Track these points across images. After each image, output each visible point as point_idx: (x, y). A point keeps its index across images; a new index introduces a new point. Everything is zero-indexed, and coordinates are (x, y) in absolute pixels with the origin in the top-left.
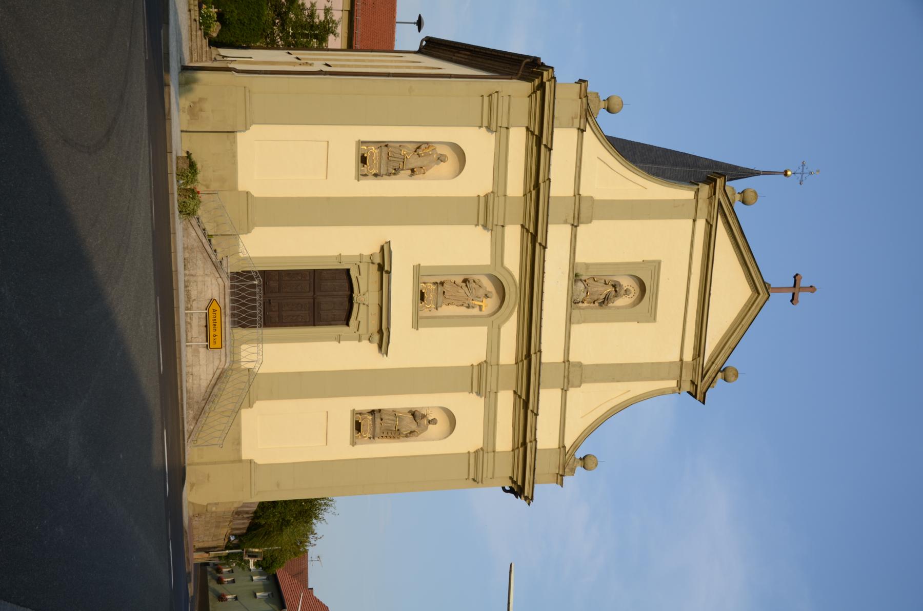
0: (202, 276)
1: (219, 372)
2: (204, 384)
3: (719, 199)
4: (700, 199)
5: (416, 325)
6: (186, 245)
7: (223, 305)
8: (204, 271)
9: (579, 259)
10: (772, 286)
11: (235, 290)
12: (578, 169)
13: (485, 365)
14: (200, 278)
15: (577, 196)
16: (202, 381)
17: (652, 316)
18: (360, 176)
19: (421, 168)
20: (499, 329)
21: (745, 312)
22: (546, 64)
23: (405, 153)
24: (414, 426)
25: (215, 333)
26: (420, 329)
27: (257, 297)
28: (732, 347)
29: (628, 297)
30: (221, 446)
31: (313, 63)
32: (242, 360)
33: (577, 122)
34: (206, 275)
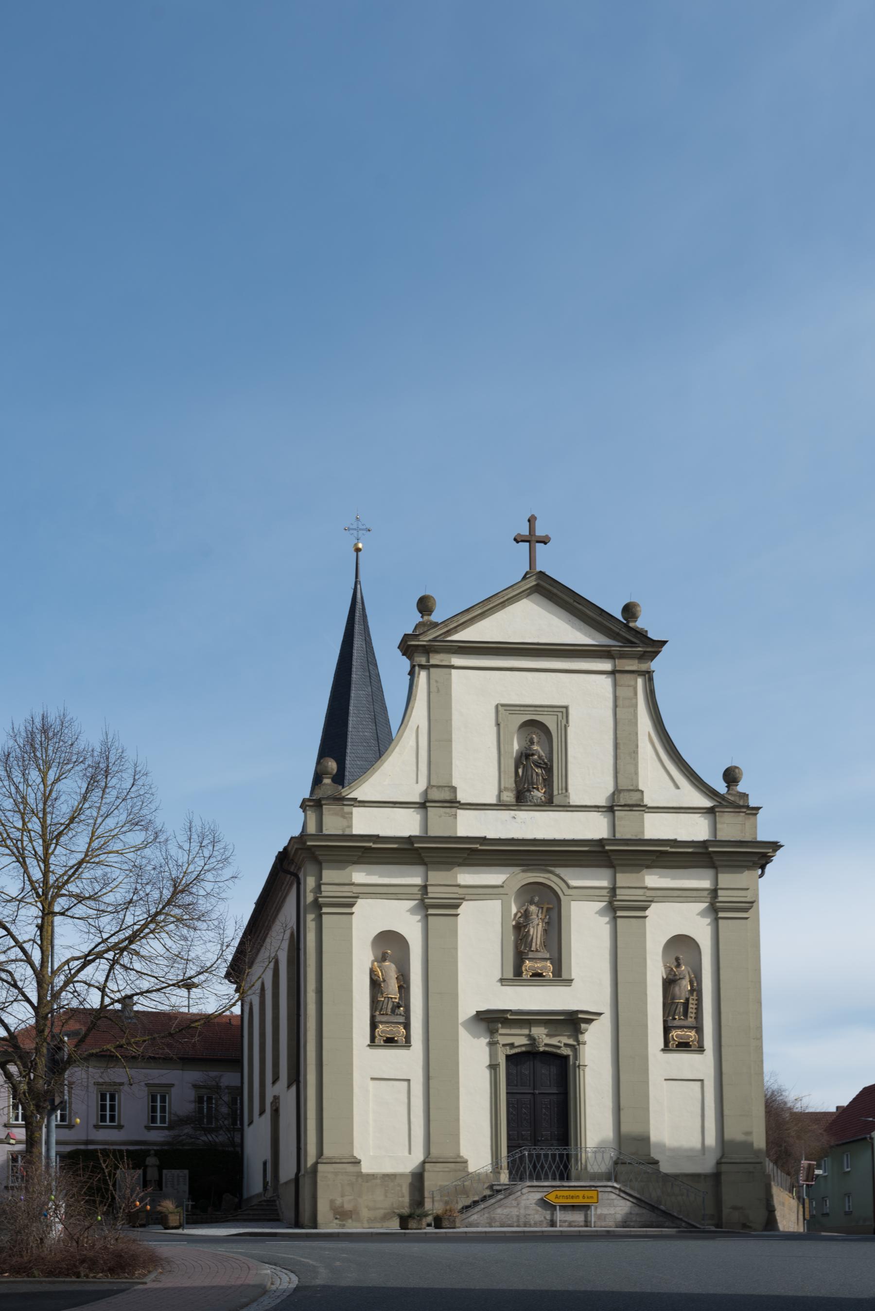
3: (430, 641)
5: (569, 982)
6: (487, 1225)
7: (550, 1188)
10: (528, 569)
12: (397, 805)
16: (633, 1212)
21: (518, 586)
22: (286, 845)
33: (346, 809)
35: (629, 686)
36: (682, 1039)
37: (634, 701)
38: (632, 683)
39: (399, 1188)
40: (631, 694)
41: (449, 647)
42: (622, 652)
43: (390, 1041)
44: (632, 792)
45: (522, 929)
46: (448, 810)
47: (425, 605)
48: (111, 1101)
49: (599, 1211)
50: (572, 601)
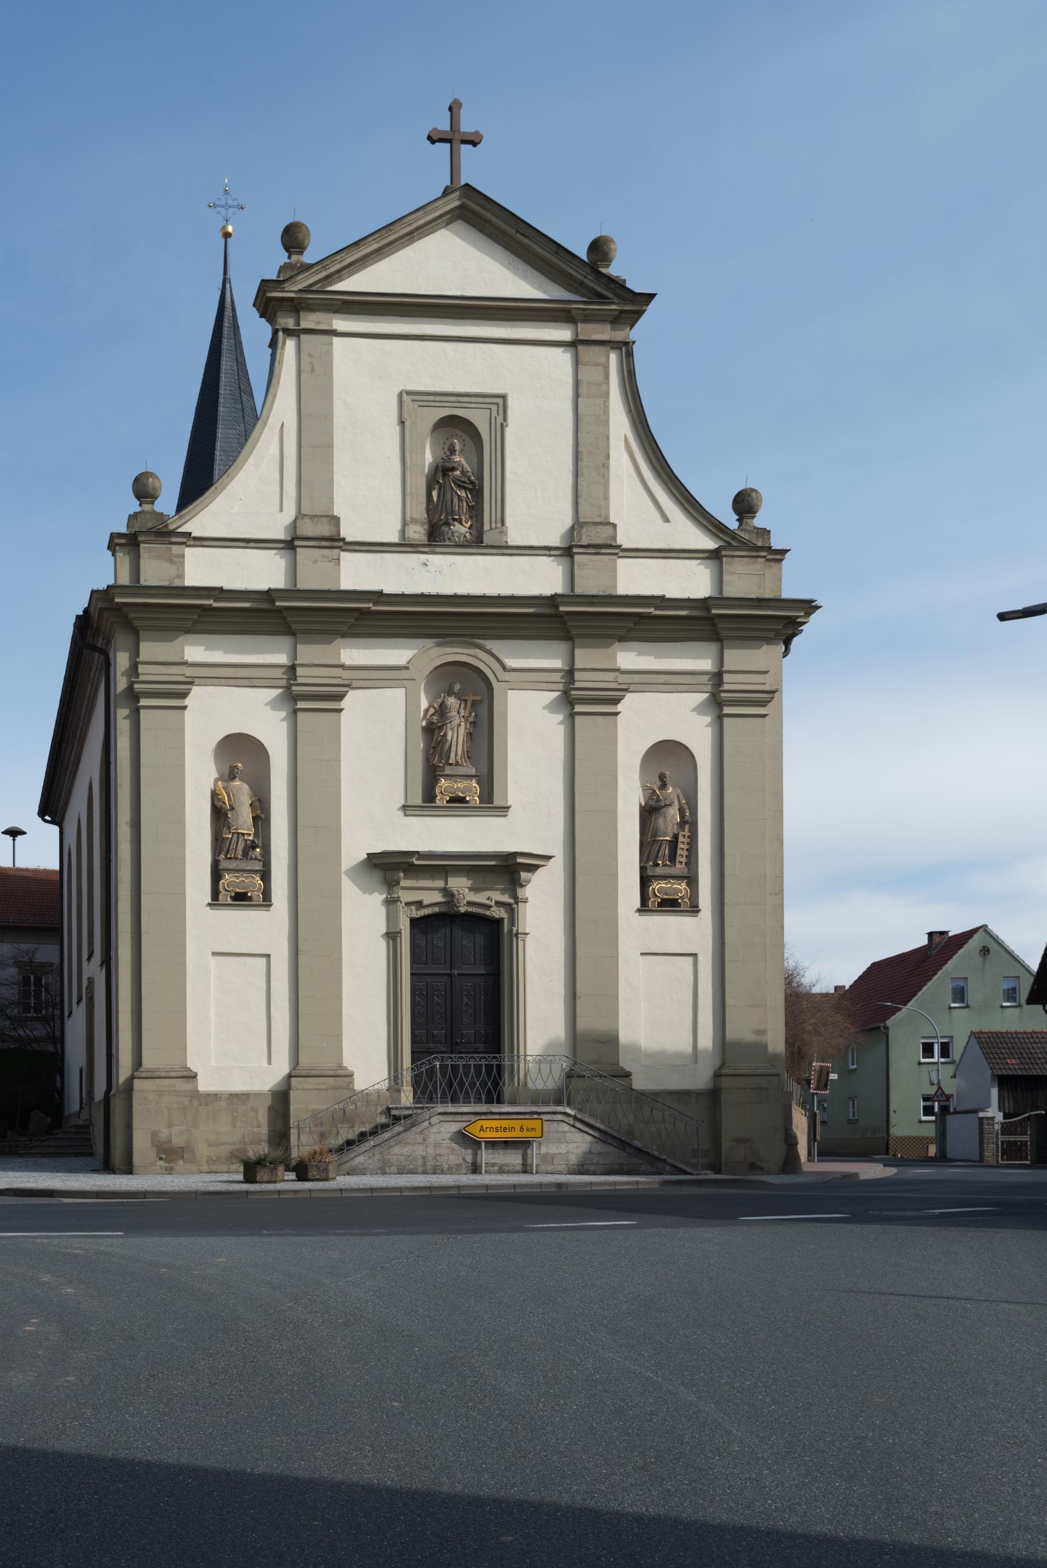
3: (300, 291)
5: (503, 810)
7: (472, 1116)
8: (419, 1144)
10: (449, 184)
12: (251, 545)
14: (429, 1150)
22: (87, 605)
25: (518, 1129)
26: (509, 804)
28: (555, 250)
31: (89, 979)
33: (175, 549)
34: (424, 1140)
35: (597, 365)
36: (666, 894)
37: (604, 387)
38: (602, 360)
39: (253, 1114)
40: (601, 378)
42: (587, 312)
43: (241, 898)
45: (436, 732)
46: (327, 552)
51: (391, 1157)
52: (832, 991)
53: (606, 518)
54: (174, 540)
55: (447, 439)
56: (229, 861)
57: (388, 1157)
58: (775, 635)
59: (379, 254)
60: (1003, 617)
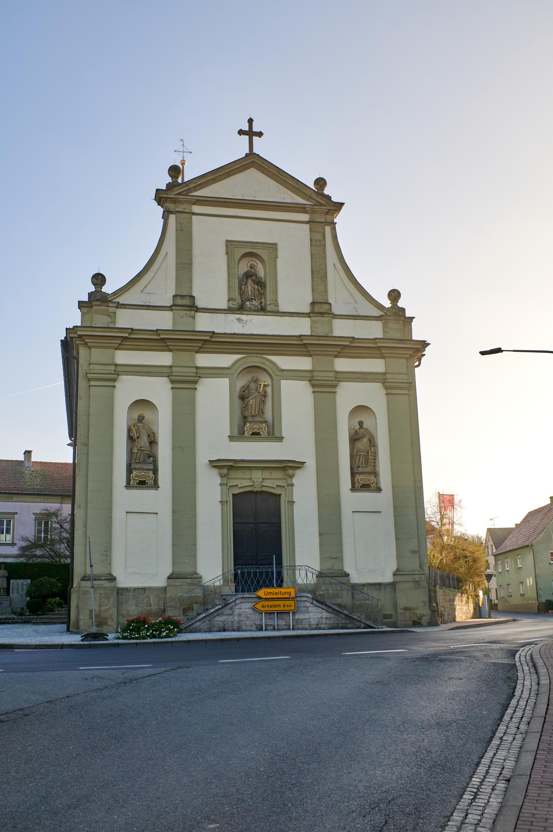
0: (234, 616)
1: (315, 602)
2: (325, 615)
3: (176, 194)
4: (175, 210)
5: (280, 439)
9: (224, 305)
11: (252, 588)
13: (386, 384)
14: (235, 618)
15: (173, 308)
17: (273, 247)
18: (155, 485)
19: (149, 435)
20: (283, 370)
23: (136, 449)
24: (365, 440)
25: (282, 605)
26: (283, 436)
27: (252, 570)
29: (256, 266)
30: (379, 600)
32: (306, 583)
33: (111, 310)
35: (319, 232)
36: (364, 482)
37: (323, 242)
38: (321, 230)
39: (148, 599)
40: (321, 238)
41: (190, 200)
42: (313, 209)
43: (142, 484)
44: (323, 304)
45: (246, 400)
46: (188, 312)
47: (175, 171)
48: (7, 525)
49: (297, 617)
50: (277, 174)
51: (214, 622)
52: (514, 526)
53: (326, 301)
54: (111, 305)
55: (247, 264)
56: (136, 464)
57: (213, 622)
58: (410, 356)
59: (214, 181)
60: (483, 353)
